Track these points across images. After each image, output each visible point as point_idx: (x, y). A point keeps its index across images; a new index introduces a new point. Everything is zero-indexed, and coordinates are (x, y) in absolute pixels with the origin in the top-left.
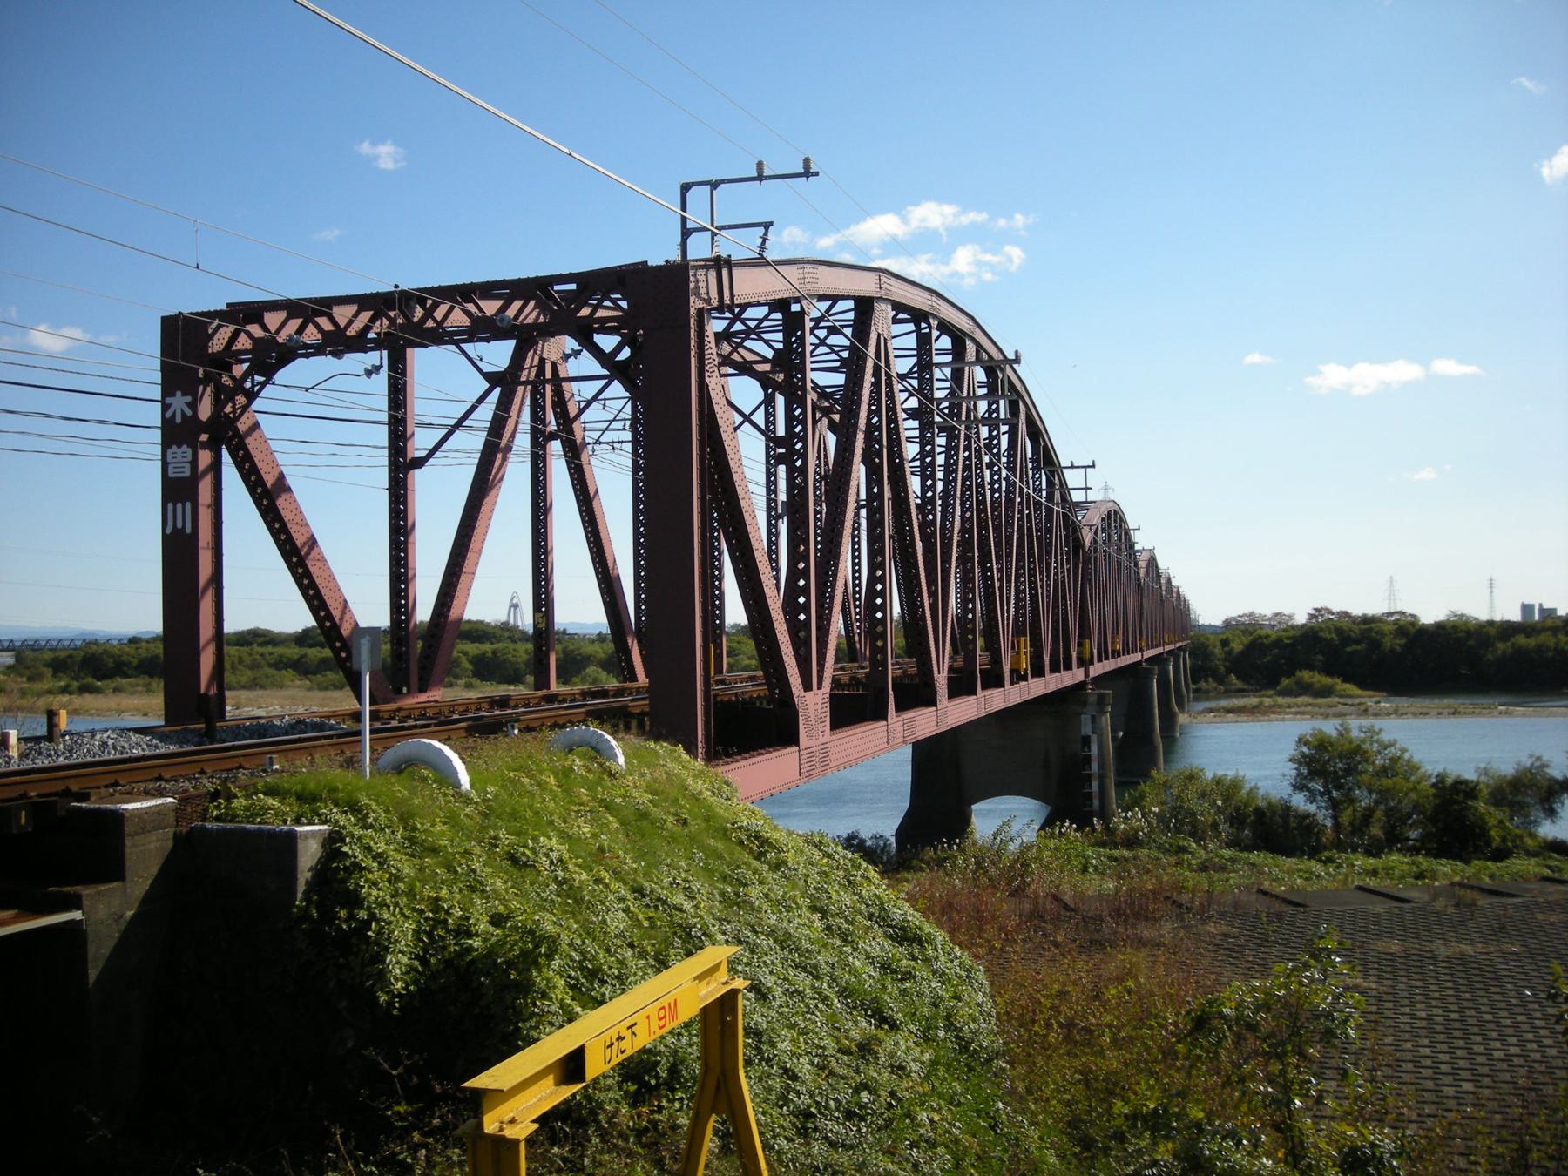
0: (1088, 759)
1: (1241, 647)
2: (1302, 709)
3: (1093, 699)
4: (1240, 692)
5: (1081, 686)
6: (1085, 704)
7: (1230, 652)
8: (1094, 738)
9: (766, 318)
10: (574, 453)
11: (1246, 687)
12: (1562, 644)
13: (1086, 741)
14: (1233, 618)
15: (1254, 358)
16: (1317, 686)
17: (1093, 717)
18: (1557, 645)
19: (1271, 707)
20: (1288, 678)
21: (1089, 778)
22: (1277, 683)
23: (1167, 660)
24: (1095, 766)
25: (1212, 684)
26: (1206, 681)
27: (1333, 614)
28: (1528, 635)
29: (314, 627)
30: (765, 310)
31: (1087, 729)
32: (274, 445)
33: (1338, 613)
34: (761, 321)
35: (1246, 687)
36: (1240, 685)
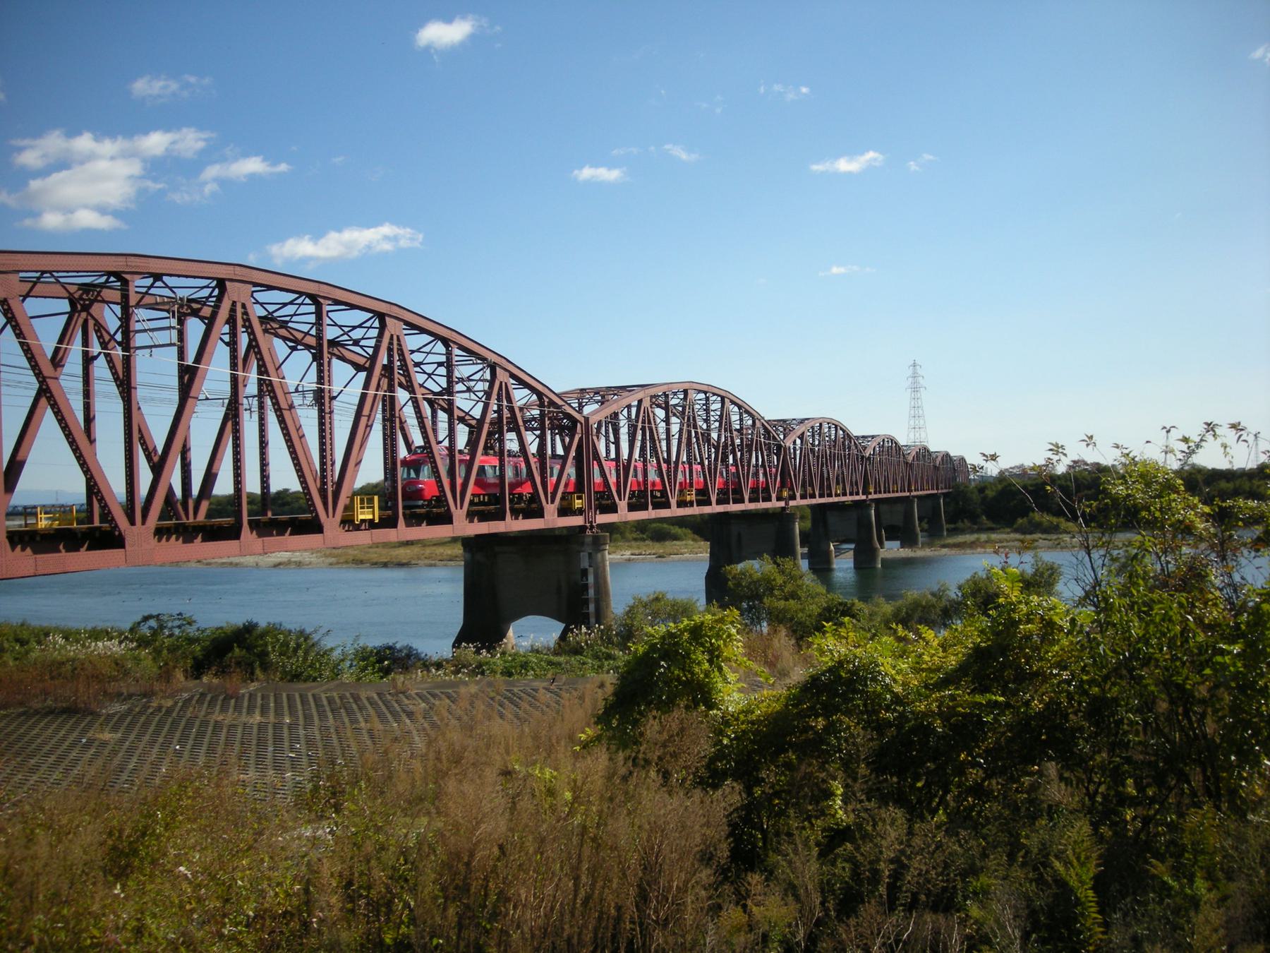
0: (586, 587)
1: (994, 494)
2: (1005, 544)
3: (588, 540)
4: (991, 530)
5: (582, 529)
6: (582, 544)
7: (985, 498)
8: (591, 570)
9: (152, 286)
10: (125, 385)
11: (994, 526)
12: (1255, 487)
13: (585, 573)
14: (1007, 470)
15: (835, 270)
16: (1046, 524)
17: (590, 554)
18: (1251, 488)
19: (987, 542)
20: (1023, 517)
21: (586, 602)
22: (1015, 520)
23: (870, 505)
24: (591, 592)
25: (967, 523)
26: (963, 521)
27: (1087, 465)
28: (1228, 481)
29: (298, 492)
30: (151, 280)
31: (585, 563)
32: (68, 396)
33: (1092, 464)
34: (149, 288)
35: (994, 526)
36: (990, 524)
